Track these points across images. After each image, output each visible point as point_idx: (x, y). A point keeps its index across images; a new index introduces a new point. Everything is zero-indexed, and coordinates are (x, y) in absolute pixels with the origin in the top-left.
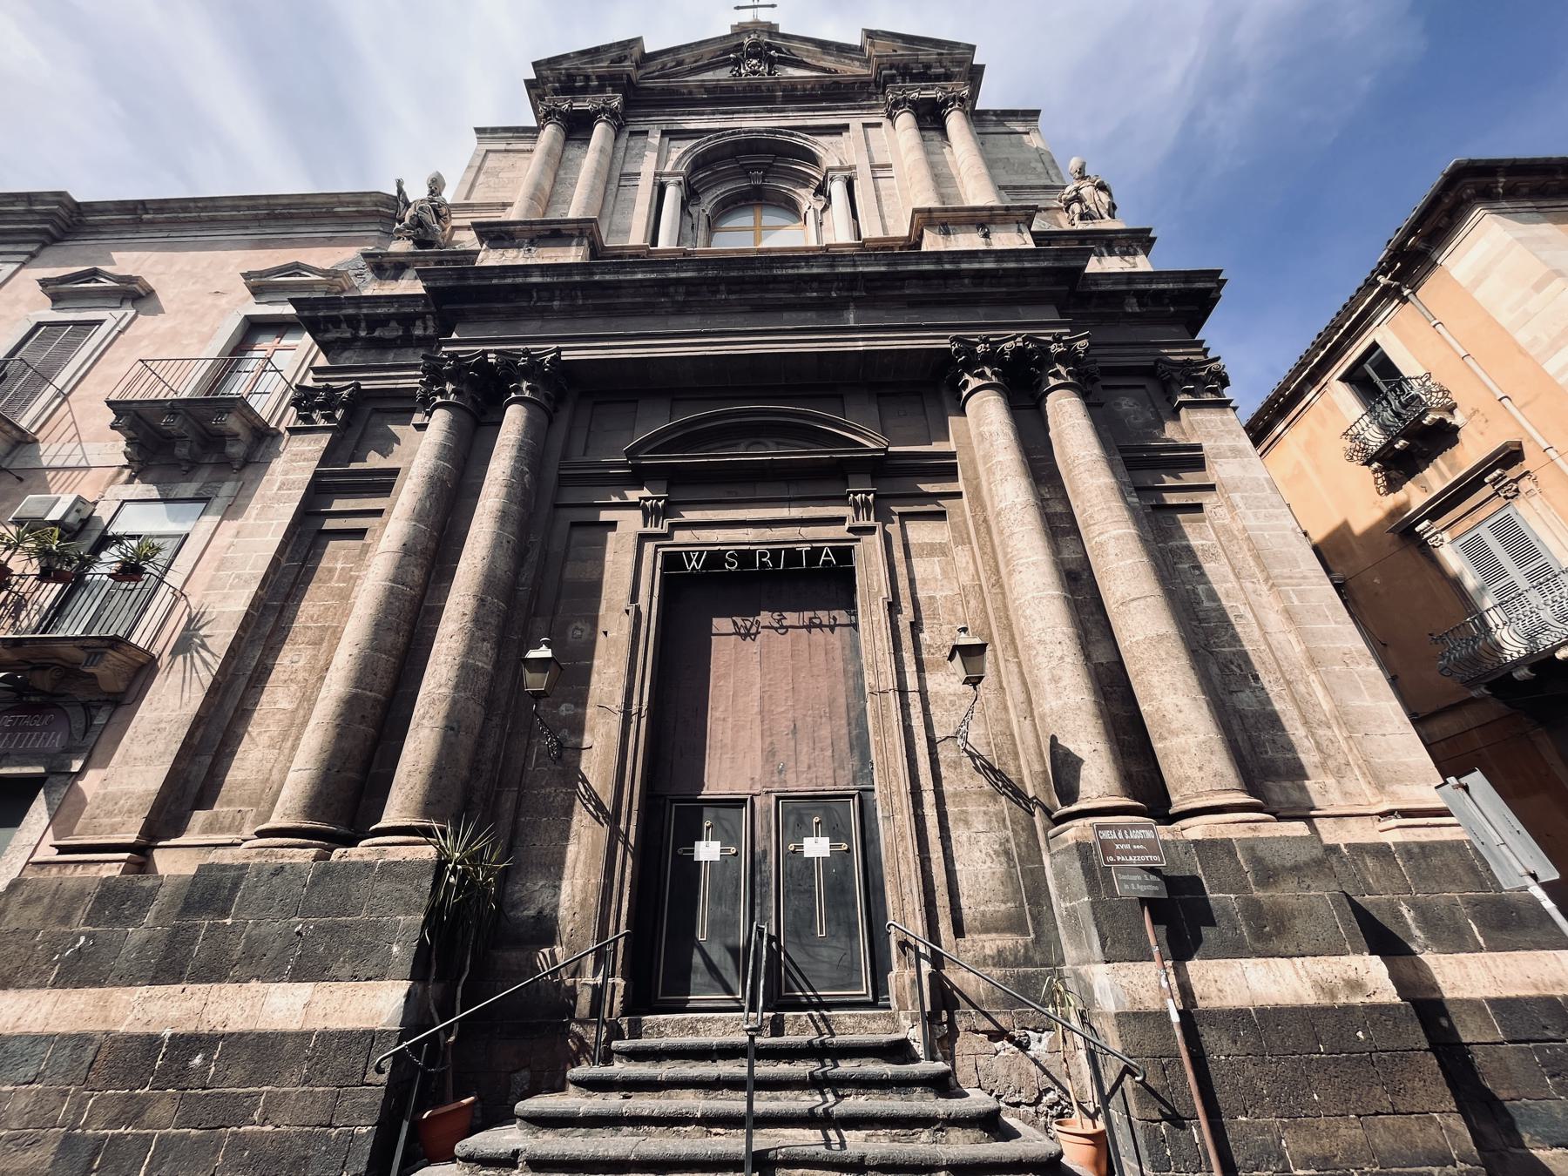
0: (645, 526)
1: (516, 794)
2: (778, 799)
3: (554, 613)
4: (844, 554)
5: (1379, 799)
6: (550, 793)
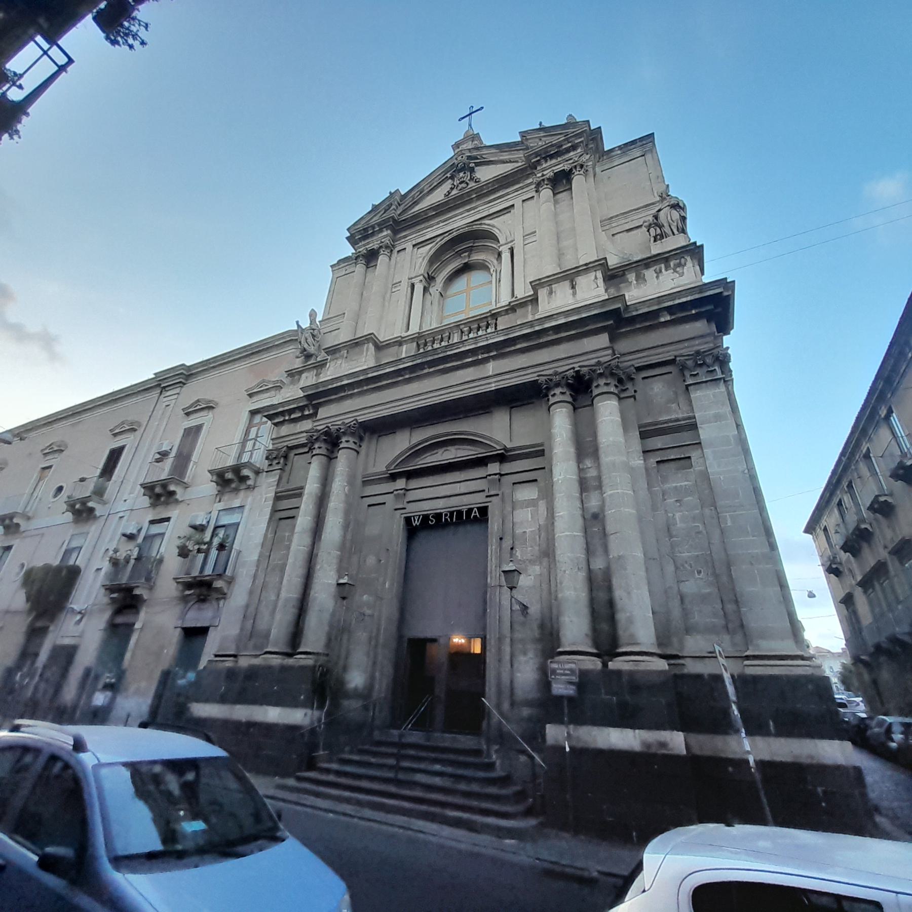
4: (484, 511)
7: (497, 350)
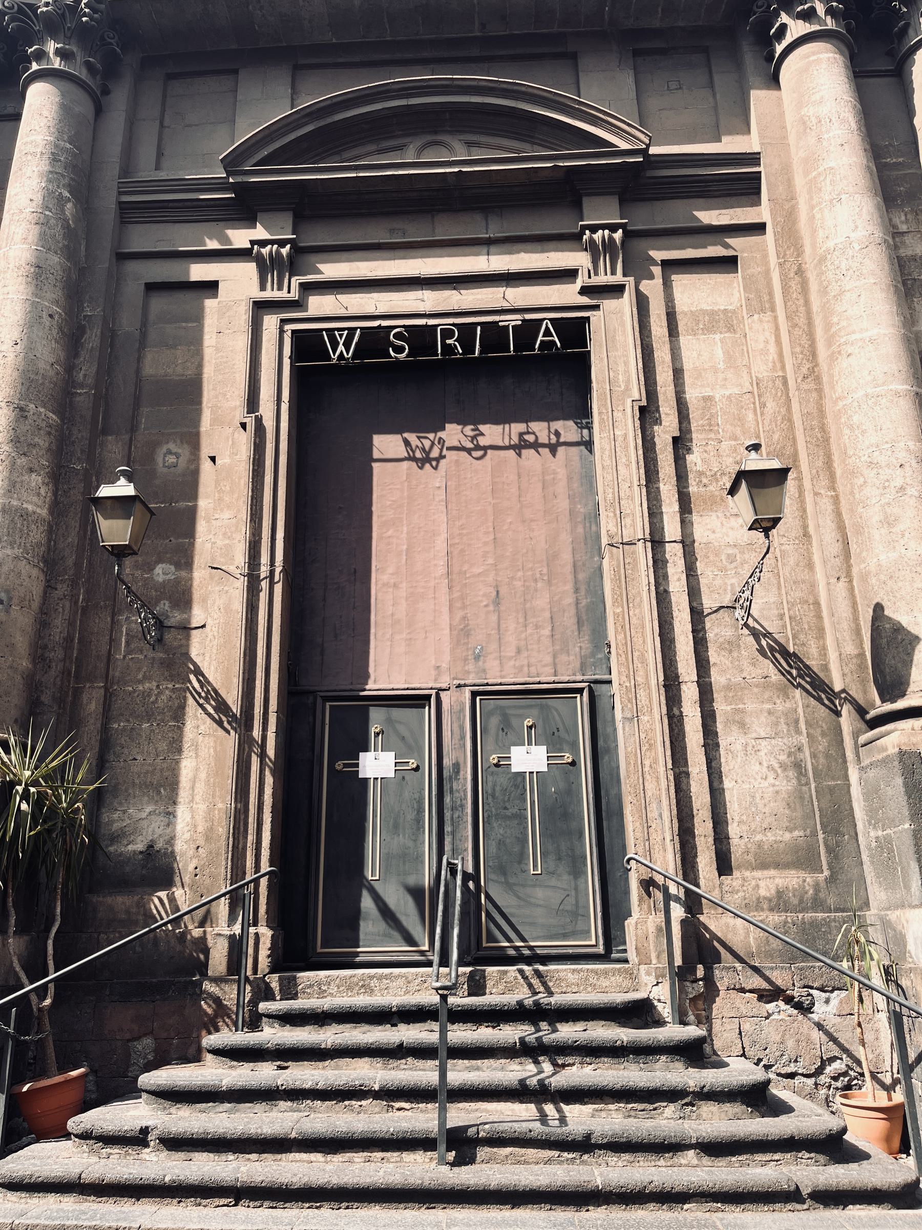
0: (263, 288)
1: (102, 691)
2: (474, 694)
3: (133, 428)
6: (152, 690)
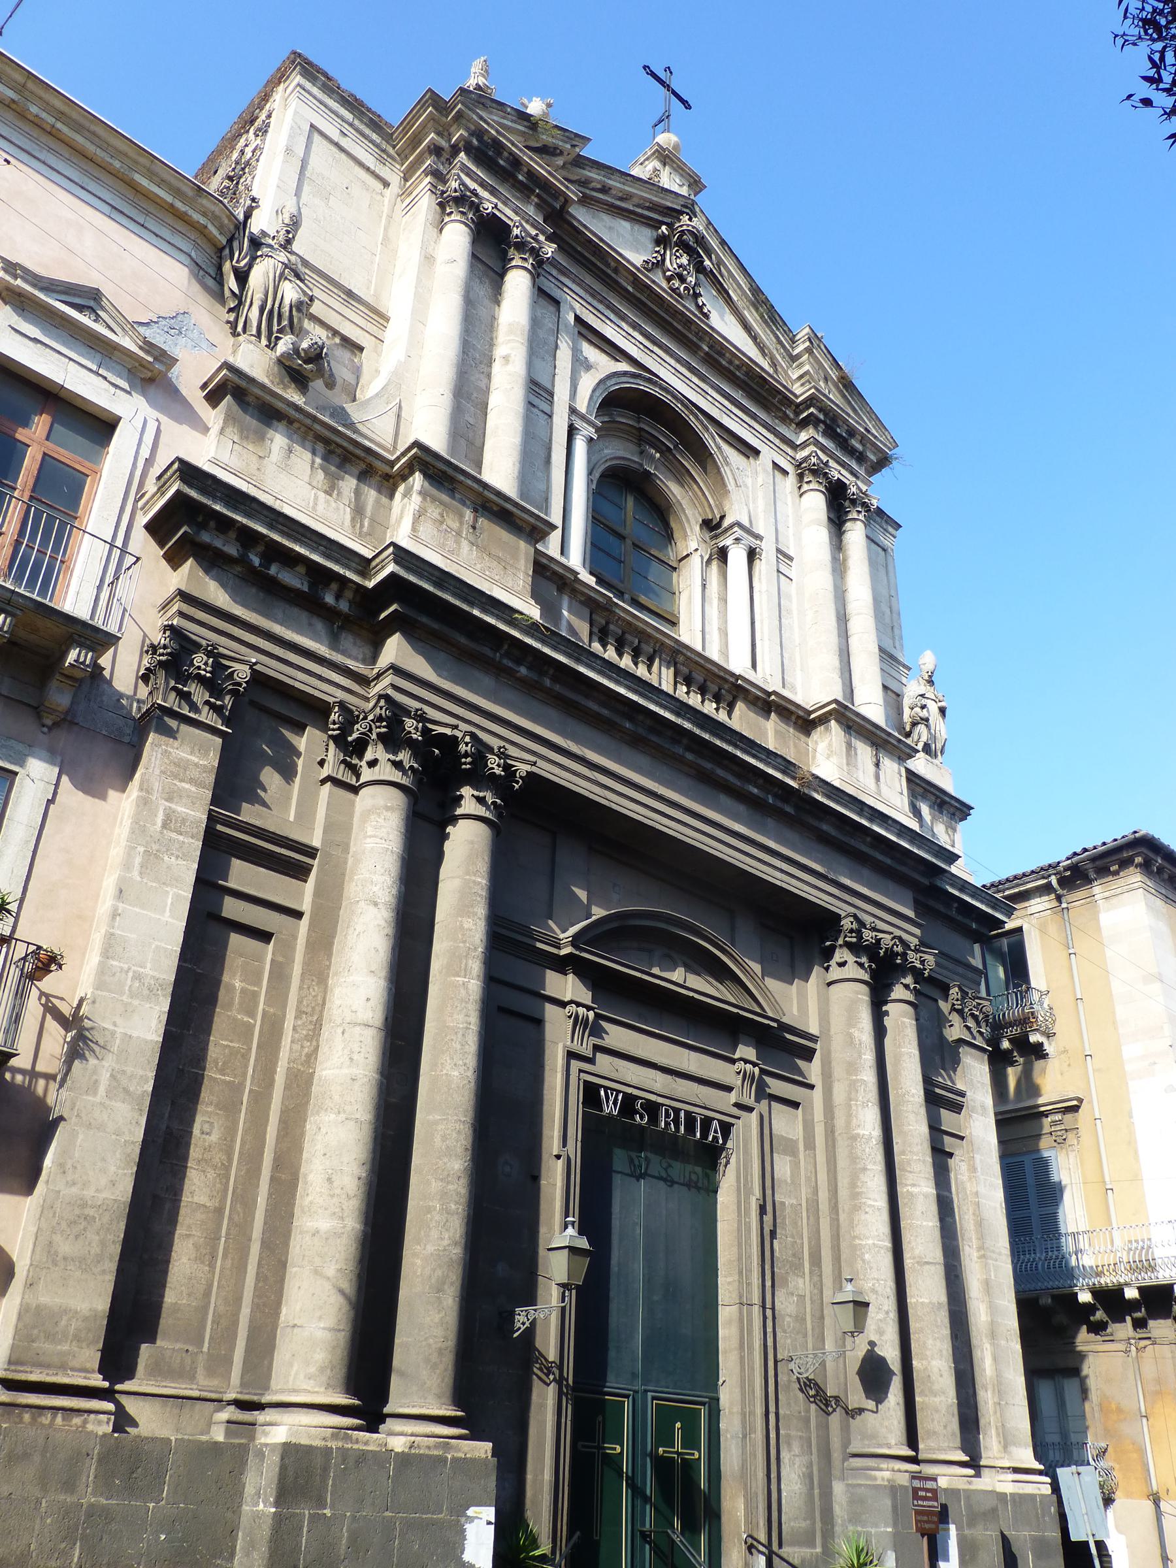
5: (1003, 1455)
7: (797, 807)
